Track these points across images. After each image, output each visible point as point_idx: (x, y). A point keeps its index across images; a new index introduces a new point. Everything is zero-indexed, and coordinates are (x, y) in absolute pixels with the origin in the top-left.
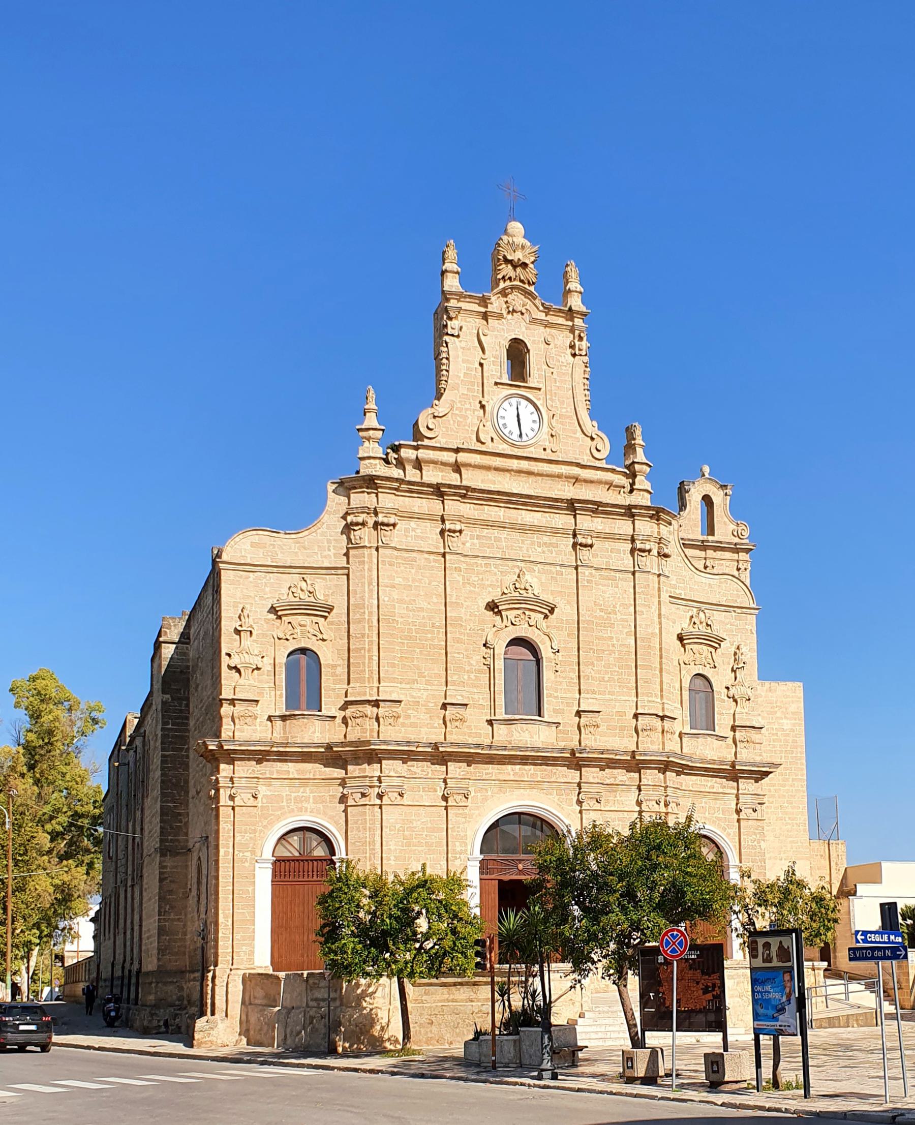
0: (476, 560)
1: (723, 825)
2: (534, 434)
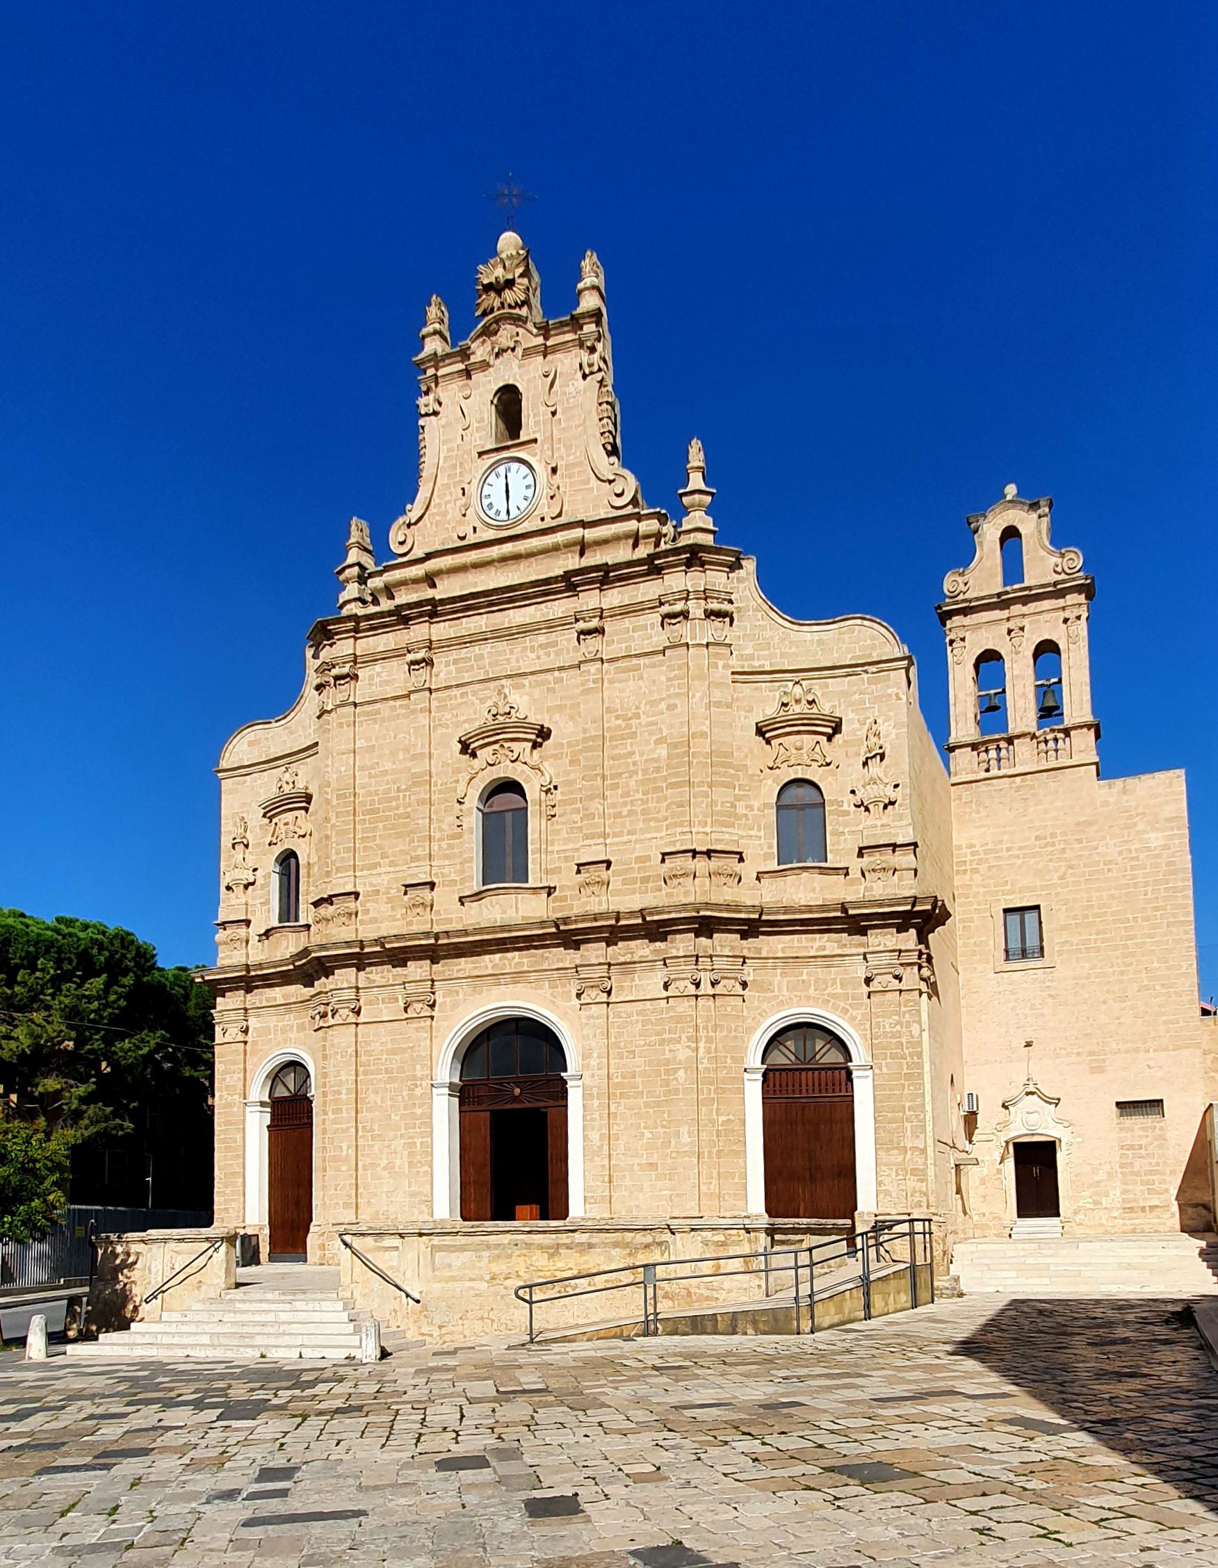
0: (447, 693)
1: (842, 1004)
2: (527, 503)
